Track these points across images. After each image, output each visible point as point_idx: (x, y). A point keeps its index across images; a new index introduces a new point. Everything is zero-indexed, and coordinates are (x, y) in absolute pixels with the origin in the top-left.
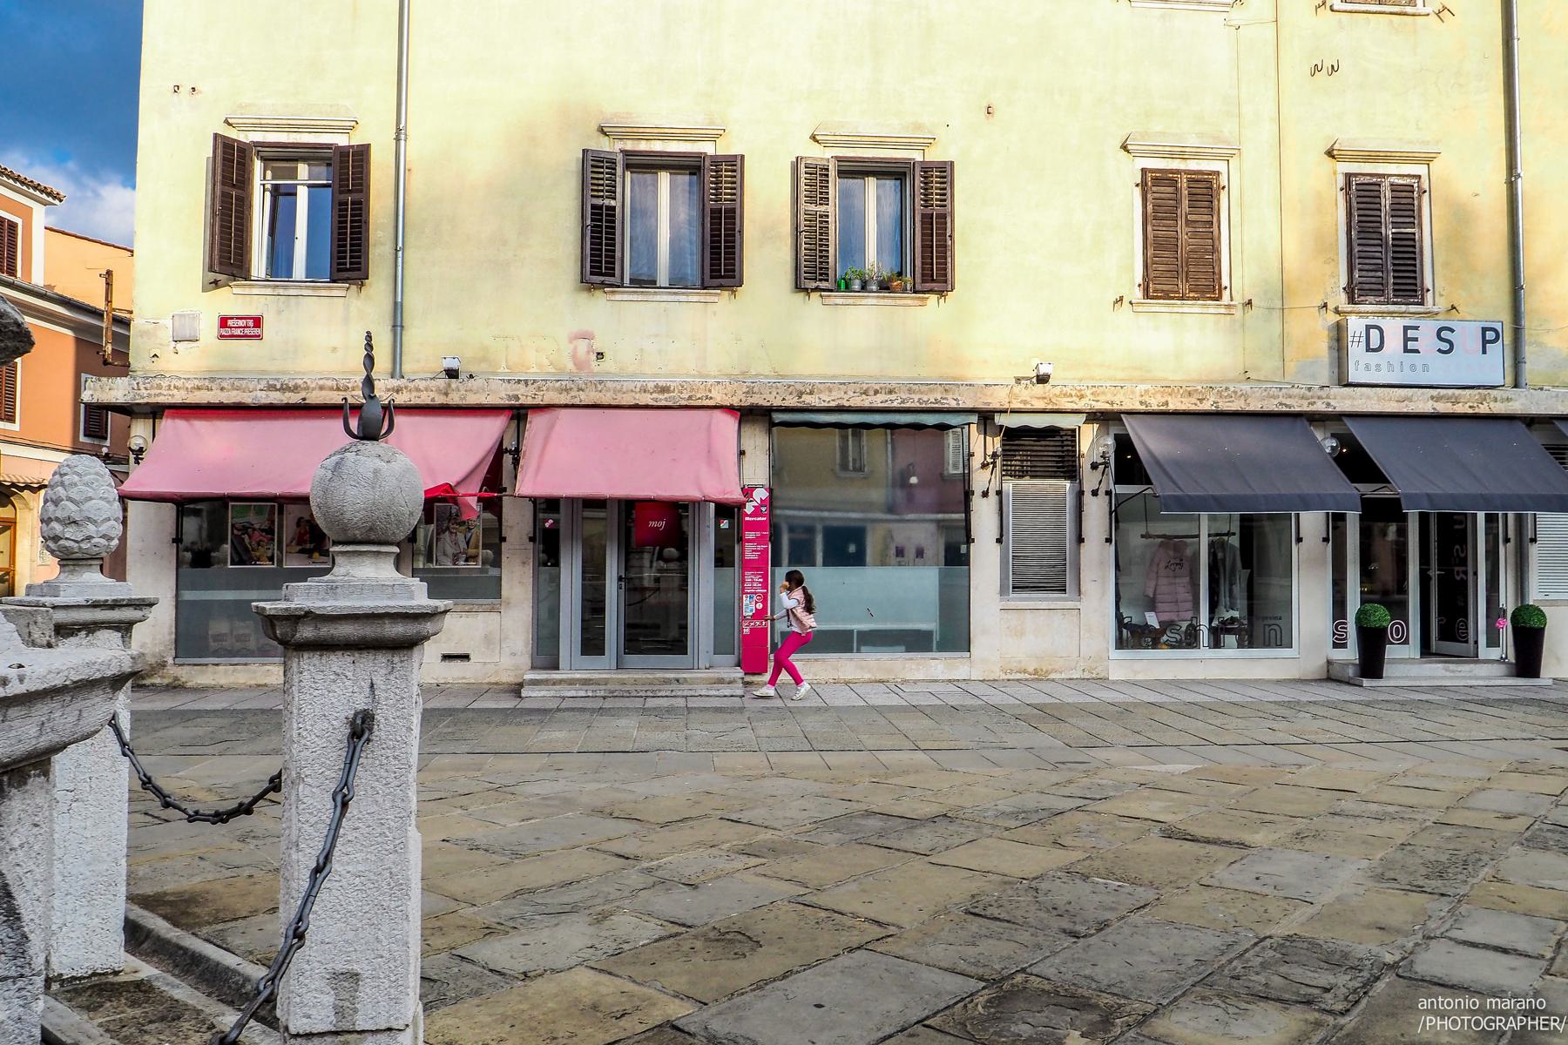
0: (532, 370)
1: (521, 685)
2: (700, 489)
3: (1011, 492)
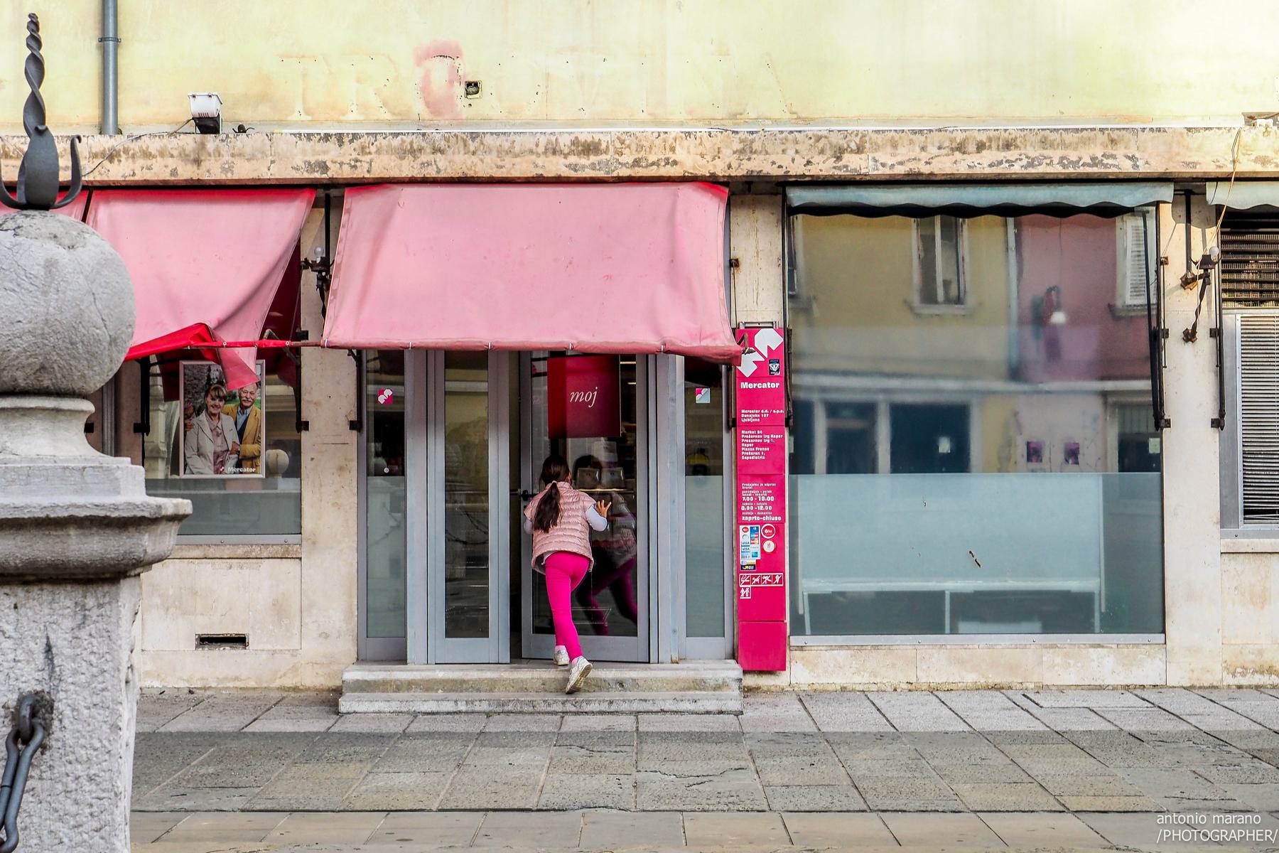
0: (351, 117)
1: (338, 691)
2: (657, 331)
3: (1239, 332)
